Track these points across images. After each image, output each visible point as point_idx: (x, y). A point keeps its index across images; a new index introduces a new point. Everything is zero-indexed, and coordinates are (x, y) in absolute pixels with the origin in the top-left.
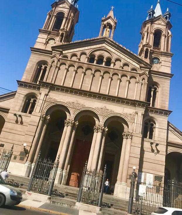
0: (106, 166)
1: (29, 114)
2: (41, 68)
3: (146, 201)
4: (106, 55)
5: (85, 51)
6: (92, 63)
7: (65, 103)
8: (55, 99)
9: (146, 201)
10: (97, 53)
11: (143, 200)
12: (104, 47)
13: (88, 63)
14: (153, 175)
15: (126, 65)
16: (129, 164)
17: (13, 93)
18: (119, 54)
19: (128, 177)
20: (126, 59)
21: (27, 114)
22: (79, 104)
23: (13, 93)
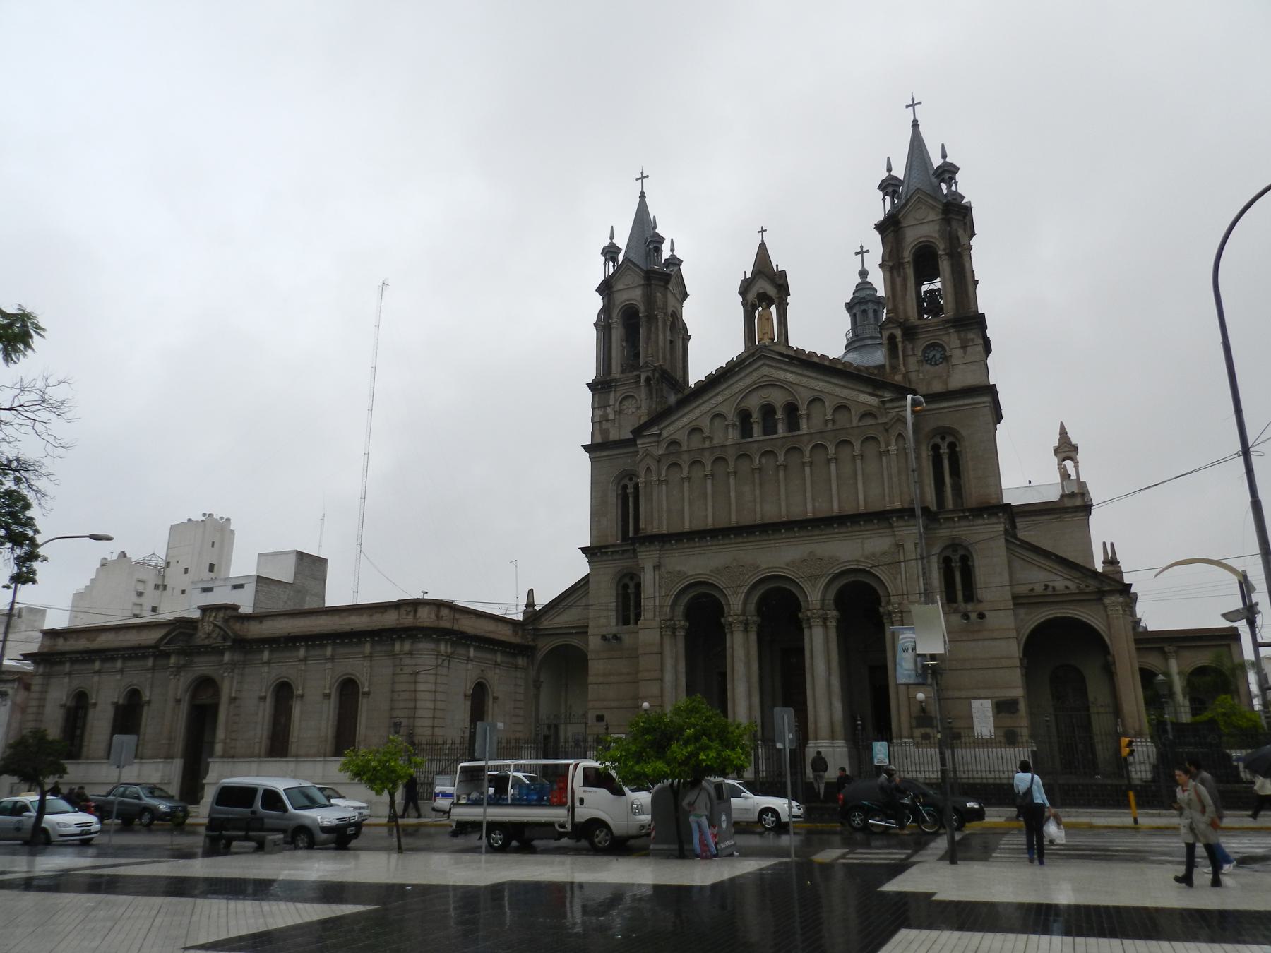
1: (625, 627)
2: (939, 453)
3: (964, 773)
4: (778, 398)
6: (795, 431)
7: (707, 575)
8: (679, 571)
10: (754, 403)
11: (902, 773)
12: (766, 379)
13: (790, 434)
14: (989, 701)
15: (841, 408)
18: (813, 383)
19: (914, 723)
20: (837, 390)
21: (631, 627)
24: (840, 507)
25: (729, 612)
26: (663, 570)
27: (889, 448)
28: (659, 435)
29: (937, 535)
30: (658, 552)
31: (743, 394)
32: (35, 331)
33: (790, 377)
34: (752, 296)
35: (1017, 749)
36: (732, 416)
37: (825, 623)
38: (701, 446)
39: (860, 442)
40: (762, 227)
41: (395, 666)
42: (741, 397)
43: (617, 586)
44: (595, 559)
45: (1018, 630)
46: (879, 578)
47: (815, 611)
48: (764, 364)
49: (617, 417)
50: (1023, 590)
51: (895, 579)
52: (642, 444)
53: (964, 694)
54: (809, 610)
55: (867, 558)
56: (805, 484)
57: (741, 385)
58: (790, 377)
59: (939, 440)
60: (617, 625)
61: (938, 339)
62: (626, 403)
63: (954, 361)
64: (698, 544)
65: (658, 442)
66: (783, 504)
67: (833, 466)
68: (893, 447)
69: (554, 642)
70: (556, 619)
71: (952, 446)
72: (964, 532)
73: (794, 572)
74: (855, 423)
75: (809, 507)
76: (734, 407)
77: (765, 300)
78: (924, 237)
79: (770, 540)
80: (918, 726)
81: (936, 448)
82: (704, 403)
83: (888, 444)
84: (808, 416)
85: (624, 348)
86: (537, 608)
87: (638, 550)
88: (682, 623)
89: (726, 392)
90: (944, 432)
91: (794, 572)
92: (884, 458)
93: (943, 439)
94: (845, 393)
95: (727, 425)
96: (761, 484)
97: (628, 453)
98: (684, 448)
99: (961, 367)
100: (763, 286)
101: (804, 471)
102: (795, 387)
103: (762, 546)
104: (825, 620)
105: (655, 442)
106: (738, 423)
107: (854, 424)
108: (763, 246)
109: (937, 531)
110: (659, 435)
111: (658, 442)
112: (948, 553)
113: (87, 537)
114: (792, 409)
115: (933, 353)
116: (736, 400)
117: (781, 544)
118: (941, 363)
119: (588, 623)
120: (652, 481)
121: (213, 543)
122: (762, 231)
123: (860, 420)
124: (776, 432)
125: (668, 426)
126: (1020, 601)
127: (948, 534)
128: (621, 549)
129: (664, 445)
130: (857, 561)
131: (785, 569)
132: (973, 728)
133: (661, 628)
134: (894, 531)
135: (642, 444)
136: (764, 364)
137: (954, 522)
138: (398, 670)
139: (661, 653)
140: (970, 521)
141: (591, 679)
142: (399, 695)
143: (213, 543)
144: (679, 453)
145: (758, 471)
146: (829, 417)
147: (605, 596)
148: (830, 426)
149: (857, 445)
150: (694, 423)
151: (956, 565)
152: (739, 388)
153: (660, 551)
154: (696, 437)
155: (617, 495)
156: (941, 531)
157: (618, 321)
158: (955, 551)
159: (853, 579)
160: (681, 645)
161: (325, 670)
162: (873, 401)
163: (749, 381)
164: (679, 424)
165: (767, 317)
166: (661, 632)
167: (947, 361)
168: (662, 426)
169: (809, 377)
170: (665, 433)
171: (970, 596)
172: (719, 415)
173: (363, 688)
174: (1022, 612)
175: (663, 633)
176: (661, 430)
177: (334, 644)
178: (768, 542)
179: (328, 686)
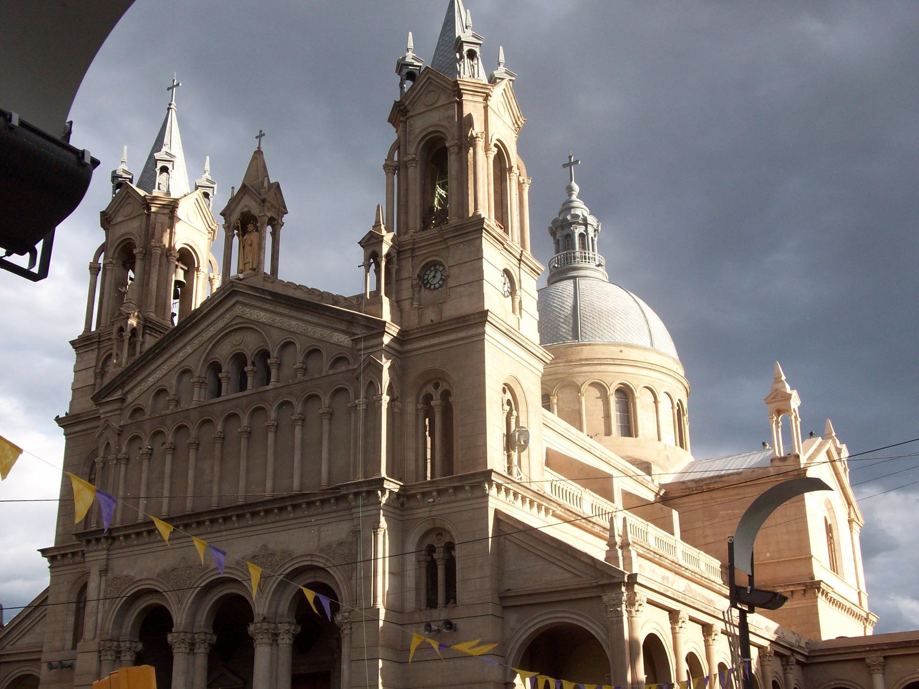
4: (249, 344)
10: (224, 352)
12: (239, 320)
15: (313, 352)
17: (270, 469)
24: (302, 484)
26: (110, 574)
27: (357, 401)
28: (122, 400)
29: (416, 516)
30: (105, 552)
32: (104, 398)
33: (263, 317)
36: (199, 369)
39: (329, 395)
40: (261, 131)
49: (98, 381)
51: (350, 579)
52: (105, 413)
55: (322, 551)
57: (212, 331)
58: (263, 317)
59: (433, 389)
65: (121, 409)
66: (242, 484)
70: (20, 642)
74: (326, 367)
75: (269, 485)
76: (203, 358)
79: (221, 531)
82: (172, 356)
83: (357, 397)
87: (353, 503)
93: (437, 386)
96: (222, 459)
100: (250, 204)
105: (117, 410)
106: (207, 381)
107: (323, 374)
108: (258, 153)
109: (415, 511)
110: (122, 400)
111: (121, 409)
112: (432, 540)
114: (264, 355)
116: (205, 351)
117: (229, 537)
122: (261, 136)
123: (332, 366)
127: (427, 514)
129: (128, 413)
130: (311, 555)
133: (100, 652)
134: (352, 514)
136: (237, 302)
150: (160, 383)
151: (438, 555)
152: (210, 335)
156: (419, 511)
163: (220, 324)
168: (126, 389)
170: (130, 399)
171: (451, 596)
172: (186, 371)
174: (512, 618)
175: (102, 659)
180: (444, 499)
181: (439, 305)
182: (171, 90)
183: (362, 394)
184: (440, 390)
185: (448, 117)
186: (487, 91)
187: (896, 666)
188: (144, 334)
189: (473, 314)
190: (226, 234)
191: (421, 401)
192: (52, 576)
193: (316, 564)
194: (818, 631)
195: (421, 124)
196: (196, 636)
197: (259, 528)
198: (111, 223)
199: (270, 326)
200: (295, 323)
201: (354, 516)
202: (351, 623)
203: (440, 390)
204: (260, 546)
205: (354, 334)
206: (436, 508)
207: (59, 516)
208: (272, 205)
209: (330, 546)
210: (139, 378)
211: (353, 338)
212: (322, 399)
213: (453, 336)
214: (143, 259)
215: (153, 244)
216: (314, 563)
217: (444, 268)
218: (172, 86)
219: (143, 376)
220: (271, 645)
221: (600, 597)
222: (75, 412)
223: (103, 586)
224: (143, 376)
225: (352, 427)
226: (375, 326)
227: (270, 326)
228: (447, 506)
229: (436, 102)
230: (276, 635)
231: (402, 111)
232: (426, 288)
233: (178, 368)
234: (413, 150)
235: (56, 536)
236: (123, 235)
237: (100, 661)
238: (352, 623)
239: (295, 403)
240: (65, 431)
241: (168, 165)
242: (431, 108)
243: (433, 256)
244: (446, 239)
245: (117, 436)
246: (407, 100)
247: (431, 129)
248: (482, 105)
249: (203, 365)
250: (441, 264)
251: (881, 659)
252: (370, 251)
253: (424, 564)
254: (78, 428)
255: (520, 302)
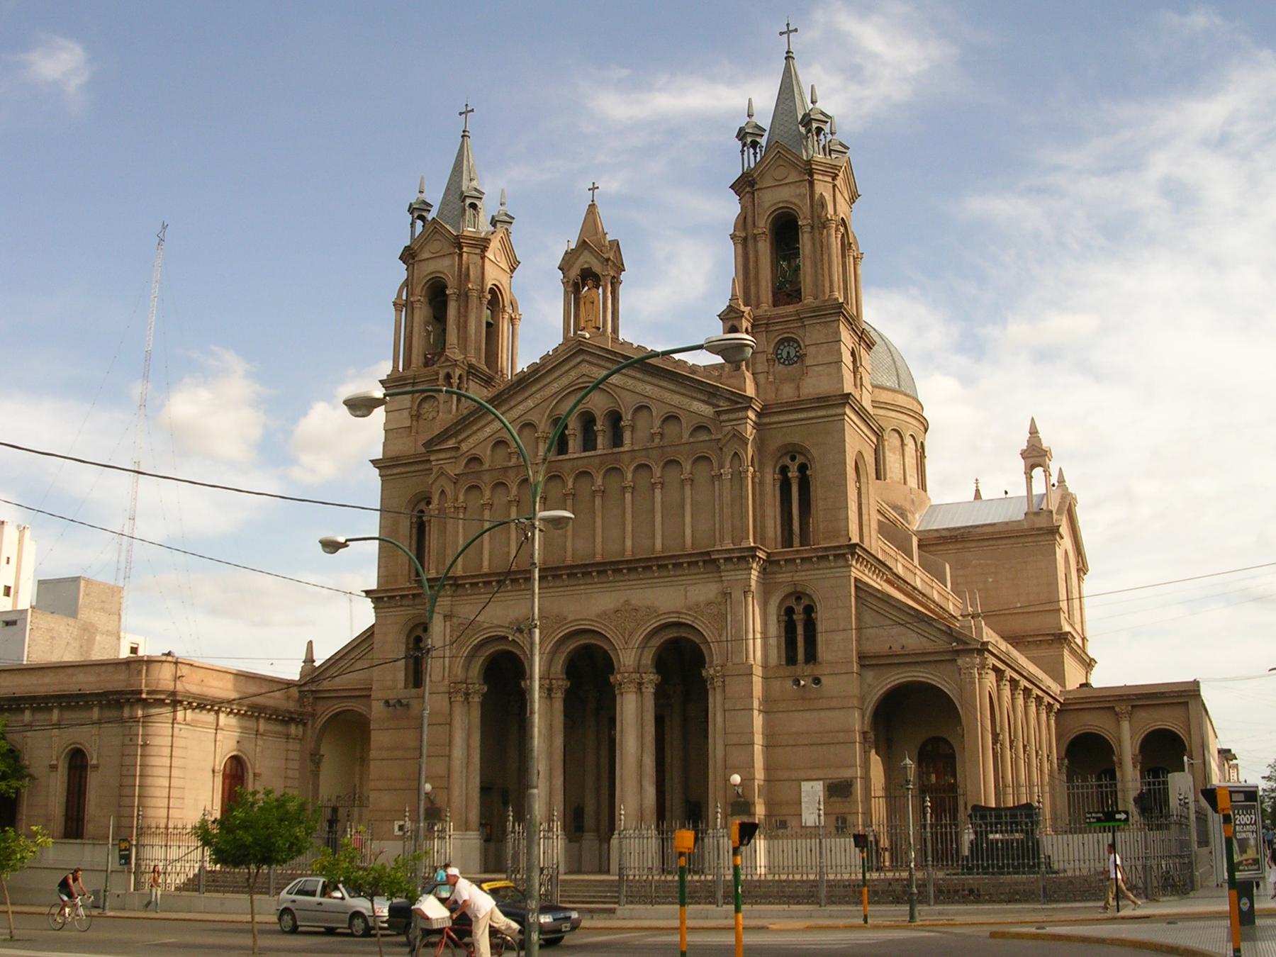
0: (511, 809)
3: (1085, 863)
4: (598, 404)
5: (473, 451)
9: (1085, 863)
14: (821, 783)
15: (671, 418)
16: (726, 768)
17: (629, 528)
18: (640, 387)
20: (667, 396)
22: (548, 618)
23: (629, 528)
25: (619, 669)
27: (722, 471)
29: (777, 581)
30: (450, 598)
31: (558, 399)
34: (574, 272)
35: (842, 840)
36: (544, 426)
37: (640, 689)
38: (505, 464)
39: (690, 462)
41: (124, 735)
42: (554, 403)
43: (408, 637)
44: (381, 605)
45: (862, 699)
46: (702, 633)
47: (626, 675)
48: (583, 361)
49: (415, 423)
50: (871, 647)
52: (437, 460)
53: (794, 775)
54: (620, 673)
55: (690, 609)
56: (624, 513)
57: (555, 387)
60: (406, 687)
61: (793, 333)
62: (426, 406)
63: (809, 361)
64: (672, 573)
66: (599, 540)
67: (658, 492)
68: (726, 470)
69: (338, 707)
71: (803, 468)
72: (812, 577)
73: (605, 625)
74: (686, 435)
75: (629, 543)
77: (588, 277)
78: (783, 202)
79: (580, 585)
80: (733, 814)
81: (784, 470)
83: (721, 466)
84: (633, 428)
85: (429, 333)
86: (317, 664)
87: (723, 567)
88: (560, 683)
89: (538, 396)
90: (793, 451)
91: (605, 625)
92: (716, 483)
93: (793, 459)
94: (676, 400)
95: (538, 438)
97: (391, 475)
98: (486, 466)
99: (816, 368)
100: (587, 260)
101: (624, 498)
102: (618, 390)
103: (694, 581)
104: (640, 685)
107: (684, 441)
108: (592, 206)
110: (457, 449)
112: (791, 602)
113: (700, 347)
114: (615, 418)
115: (786, 350)
116: (548, 407)
118: (796, 362)
119: (371, 685)
120: (446, 508)
121: (8, 563)
122: (593, 189)
123: (691, 435)
124: (595, 449)
125: (468, 437)
126: (866, 661)
127: (790, 579)
128: (411, 592)
131: (596, 621)
132: (801, 815)
133: (450, 693)
134: (721, 577)
135: (437, 460)
136: (583, 361)
137: (563, 580)
138: (127, 741)
139: (450, 724)
140: (624, 575)
141: (373, 754)
142: (128, 770)
143: (8, 563)
144: (478, 474)
145: (690, 483)
146: (655, 430)
147: (394, 645)
148: (513, 461)
149: (687, 467)
151: (799, 617)
153: (452, 596)
154: (501, 452)
155: (412, 523)
157: (422, 299)
158: (798, 598)
159: (675, 635)
160: (476, 713)
161: (51, 737)
162: (707, 410)
163: (564, 381)
164: (481, 436)
165: (591, 300)
166: (450, 698)
167: (803, 361)
168: (460, 438)
169: (634, 378)
170: (464, 447)
171: (811, 657)
173: (91, 760)
174: (870, 675)
175: (452, 699)
176: (459, 442)
177: (61, 708)
178: (577, 588)
179: (54, 757)
180: (807, 566)
181: (797, 380)
182: (464, 116)
183: (727, 464)
184: (797, 462)
185: (800, 195)
186: (837, 172)
187: (1142, 715)
188: (468, 379)
189: (835, 396)
190: (565, 290)
191: (777, 471)
192: (376, 617)
193: (684, 621)
194: (380, 544)
195: (772, 198)
196: (554, 682)
197: (621, 584)
198: (416, 259)
199: (622, 388)
200: (648, 388)
201: (723, 578)
202: (724, 676)
203: (797, 462)
204: (622, 601)
205: (719, 406)
206: (798, 574)
207: (379, 558)
208: (614, 264)
209: (697, 605)
210: (475, 428)
211: (717, 410)
212: (683, 465)
213: (812, 414)
214: (457, 301)
215: (470, 286)
216: (694, 625)
217: (799, 346)
218: (469, 114)
219: (479, 425)
220: (636, 693)
221: (956, 660)
222: (393, 454)
223: (448, 631)
224: (479, 425)
225: (717, 493)
226: (740, 400)
227: (622, 388)
228: (808, 573)
229: (786, 177)
230: (640, 684)
231: (750, 181)
232: (780, 363)
233: (519, 420)
234: (763, 225)
235: (378, 577)
236: (432, 273)
237: (451, 703)
238: (725, 676)
239: (654, 468)
240: (380, 472)
241: (477, 203)
242: (780, 184)
243: (788, 333)
244: (801, 319)
245: (453, 485)
246: (755, 172)
247: (781, 205)
248: (831, 185)
249: (547, 421)
250: (796, 341)
251: (1130, 708)
252: (730, 324)
253: (783, 625)
254: (395, 471)
255: (861, 378)
